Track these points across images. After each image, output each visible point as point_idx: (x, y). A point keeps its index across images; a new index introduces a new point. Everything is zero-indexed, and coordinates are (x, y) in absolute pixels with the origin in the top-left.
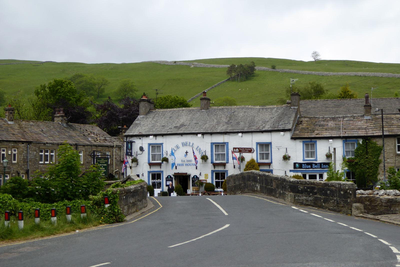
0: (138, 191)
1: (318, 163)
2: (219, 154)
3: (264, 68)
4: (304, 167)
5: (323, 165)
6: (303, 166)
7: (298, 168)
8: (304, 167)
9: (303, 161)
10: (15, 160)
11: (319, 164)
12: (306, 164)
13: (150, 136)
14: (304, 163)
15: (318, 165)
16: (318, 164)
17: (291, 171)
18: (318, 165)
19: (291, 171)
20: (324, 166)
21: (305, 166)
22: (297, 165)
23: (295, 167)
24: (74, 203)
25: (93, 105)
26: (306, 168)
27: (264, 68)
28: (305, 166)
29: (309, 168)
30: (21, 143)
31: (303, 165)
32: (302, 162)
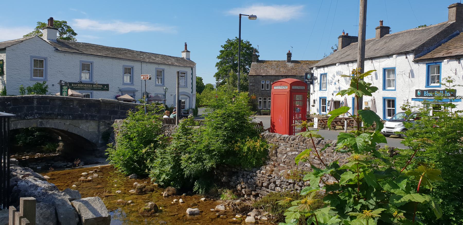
0: (429, 176)
1: (441, 90)
2: (435, 75)
3: (6, 184)
4: (425, 95)
5: (447, 92)
6: (425, 94)
7: (420, 96)
8: (425, 95)
9: (425, 88)
10: (263, 88)
11: (442, 91)
12: (427, 92)
13: (394, 56)
14: (426, 91)
15: (442, 92)
16: (441, 91)
17: (413, 99)
18: (442, 92)
19: (413, 99)
20: (448, 93)
21: (427, 93)
22: (419, 92)
23: (417, 95)
24: (274, 190)
25: (136, 147)
26: (427, 96)
27: (6, 184)
28: (427, 93)
29: (431, 97)
30: (281, 77)
31: (425, 92)
32: (424, 88)
